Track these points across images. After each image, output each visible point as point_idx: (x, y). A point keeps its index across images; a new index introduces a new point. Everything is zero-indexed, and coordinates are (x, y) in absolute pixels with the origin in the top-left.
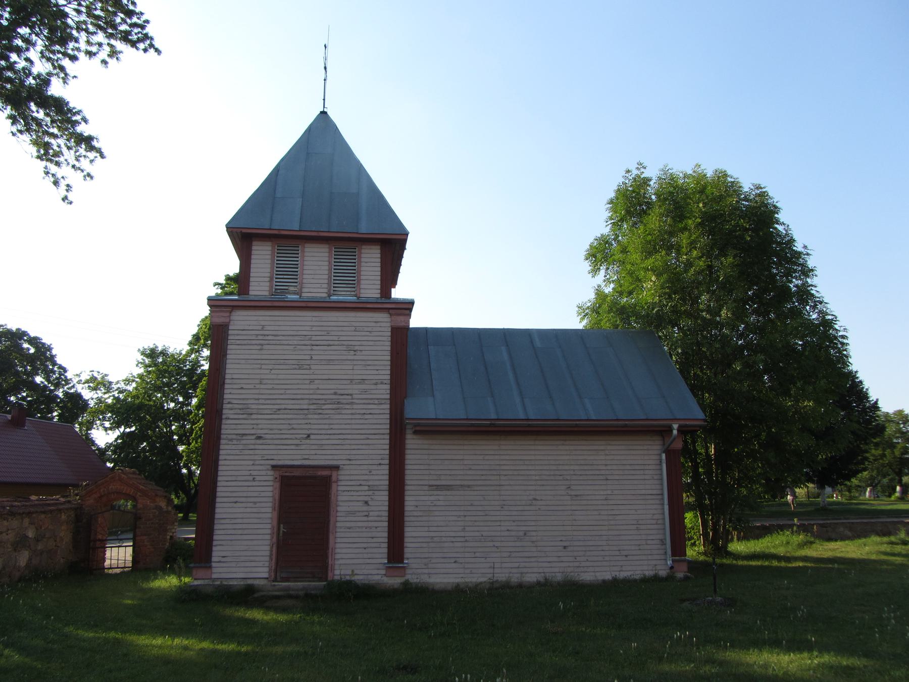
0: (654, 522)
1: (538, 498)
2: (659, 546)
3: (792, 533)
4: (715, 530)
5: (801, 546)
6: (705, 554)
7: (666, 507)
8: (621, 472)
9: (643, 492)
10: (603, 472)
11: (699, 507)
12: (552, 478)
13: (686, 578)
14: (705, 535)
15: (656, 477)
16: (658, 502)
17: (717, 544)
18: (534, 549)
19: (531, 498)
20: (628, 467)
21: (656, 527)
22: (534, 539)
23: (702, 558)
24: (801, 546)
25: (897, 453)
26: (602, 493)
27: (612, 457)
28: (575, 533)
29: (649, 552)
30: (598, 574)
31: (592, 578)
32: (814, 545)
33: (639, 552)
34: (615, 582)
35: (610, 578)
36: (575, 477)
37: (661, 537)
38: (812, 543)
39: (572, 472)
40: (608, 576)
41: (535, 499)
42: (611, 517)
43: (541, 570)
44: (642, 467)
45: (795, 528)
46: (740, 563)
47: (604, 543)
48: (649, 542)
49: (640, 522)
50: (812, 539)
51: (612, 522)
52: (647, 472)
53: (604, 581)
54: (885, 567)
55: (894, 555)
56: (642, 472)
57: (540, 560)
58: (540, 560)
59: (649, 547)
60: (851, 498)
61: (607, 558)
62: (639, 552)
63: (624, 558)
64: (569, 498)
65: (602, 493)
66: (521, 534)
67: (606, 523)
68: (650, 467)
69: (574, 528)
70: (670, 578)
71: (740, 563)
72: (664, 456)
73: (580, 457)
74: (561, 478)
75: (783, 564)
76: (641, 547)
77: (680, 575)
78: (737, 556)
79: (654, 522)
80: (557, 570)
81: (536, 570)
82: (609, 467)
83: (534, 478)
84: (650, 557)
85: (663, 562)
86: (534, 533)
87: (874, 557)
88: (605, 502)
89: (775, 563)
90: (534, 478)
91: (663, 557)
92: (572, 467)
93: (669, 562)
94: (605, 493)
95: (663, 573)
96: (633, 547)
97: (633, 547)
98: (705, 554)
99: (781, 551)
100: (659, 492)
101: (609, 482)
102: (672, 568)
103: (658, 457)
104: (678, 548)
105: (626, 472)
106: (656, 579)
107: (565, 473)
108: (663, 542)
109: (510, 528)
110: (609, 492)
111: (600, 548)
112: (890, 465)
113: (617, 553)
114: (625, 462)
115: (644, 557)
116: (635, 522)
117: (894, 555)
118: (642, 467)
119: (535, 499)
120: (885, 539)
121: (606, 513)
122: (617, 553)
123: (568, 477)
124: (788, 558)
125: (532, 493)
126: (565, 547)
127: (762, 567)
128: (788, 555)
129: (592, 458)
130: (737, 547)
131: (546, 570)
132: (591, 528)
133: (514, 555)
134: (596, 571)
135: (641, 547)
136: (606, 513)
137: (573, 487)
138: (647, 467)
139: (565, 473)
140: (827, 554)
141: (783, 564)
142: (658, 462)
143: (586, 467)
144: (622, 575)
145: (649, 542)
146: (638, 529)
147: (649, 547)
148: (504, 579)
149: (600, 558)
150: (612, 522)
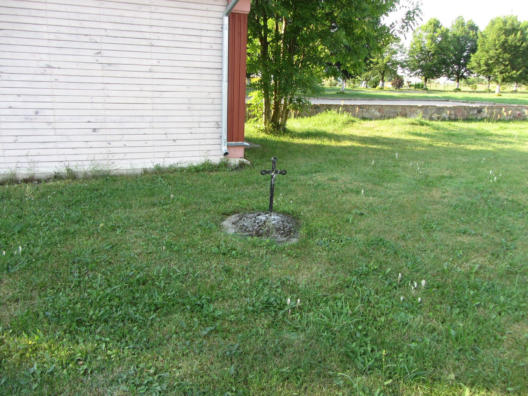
0: (210, 101)
1: (53, 64)
2: (214, 130)
3: (338, 112)
4: (277, 108)
5: (347, 123)
6: (265, 131)
7: (225, 85)
8: (171, 37)
9: (198, 65)
10: (147, 36)
11: (264, 86)
12: (74, 38)
13: (242, 165)
14: (267, 113)
15: (215, 47)
16: (216, 77)
17: (277, 126)
18: (52, 132)
19: (43, 64)
20: (181, 31)
21: (212, 107)
22: (51, 119)
23: (262, 135)
24: (347, 123)
25: (385, 61)
26: (144, 62)
27: (159, 16)
28: (108, 113)
29: (202, 136)
30: (134, 162)
31: (129, 167)
32: (355, 124)
33: (189, 136)
34: (159, 171)
35: (152, 167)
36: (107, 40)
37: (217, 119)
38: (353, 121)
39: (103, 33)
40: (150, 165)
41: (49, 67)
42: (156, 94)
43: (62, 158)
44: (198, 33)
45: (340, 109)
46: (297, 141)
47: (147, 125)
48: (202, 125)
49: (193, 101)
50: (353, 119)
51: (158, 101)
52: (204, 40)
53: (145, 171)
54: (419, 148)
55: (420, 135)
56: (198, 39)
57: (61, 145)
58: (61, 145)
59: (202, 130)
60: (354, 87)
61: (150, 143)
62: (189, 136)
63: (172, 143)
64: (99, 67)
65: (144, 62)
66: (32, 112)
67: (149, 101)
68: (209, 34)
69: (107, 106)
70: (224, 166)
71: (297, 141)
72: (226, 19)
73: (114, 12)
74: (87, 39)
75: (333, 143)
76: (193, 130)
77: (235, 161)
78: (293, 134)
79: (210, 101)
80: (85, 157)
81: (55, 158)
82: (154, 29)
83: (46, 36)
84: (203, 142)
85: (218, 147)
86: (50, 112)
87: (404, 137)
88: (149, 75)
89: (326, 142)
90: (46, 36)
91: (218, 141)
92: (103, 26)
93: (224, 149)
94: (149, 62)
95: (216, 159)
96: (183, 131)
97: (183, 131)
98: (265, 131)
99: (329, 129)
100: (218, 66)
101: (154, 49)
102: (226, 154)
103: (219, 21)
104: (234, 132)
105: (178, 38)
106: (207, 168)
107: (93, 32)
108: (218, 125)
109: (13, 105)
110: (155, 62)
111: (142, 131)
112: (379, 68)
113: (164, 137)
114: (176, 24)
115: (197, 142)
116: (186, 101)
117: (420, 135)
118: (198, 33)
119: (49, 67)
120: (408, 120)
121: (150, 88)
122: (164, 137)
123: (98, 39)
124: (336, 136)
125: (44, 57)
126: (94, 130)
127: (315, 146)
128: (335, 133)
129: (132, 14)
130: (294, 124)
131: (69, 158)
132: (131, 106)
133: (20, 139)
134: (132, 159)
135: (193, 130)
136: (150, 88)
137: (104, 53)
138: (204, 33)
139: (93, 32)
140: (368, 134)
141: (333, 143)
142: (219, 28)
143: (123, 27)
144: (167, 163)
145: (202, 125)
146: (189, 109)
147: (202, 130)
148: (8, 171)
149: (142, 143)
150: (158, 101)
